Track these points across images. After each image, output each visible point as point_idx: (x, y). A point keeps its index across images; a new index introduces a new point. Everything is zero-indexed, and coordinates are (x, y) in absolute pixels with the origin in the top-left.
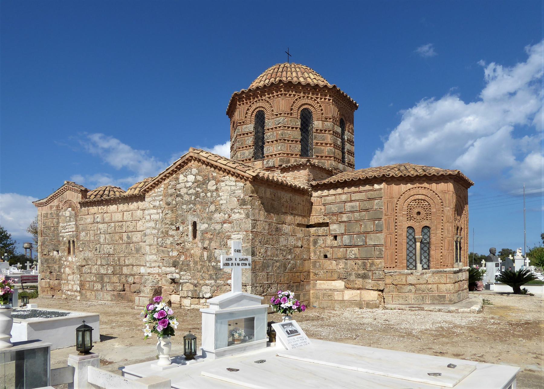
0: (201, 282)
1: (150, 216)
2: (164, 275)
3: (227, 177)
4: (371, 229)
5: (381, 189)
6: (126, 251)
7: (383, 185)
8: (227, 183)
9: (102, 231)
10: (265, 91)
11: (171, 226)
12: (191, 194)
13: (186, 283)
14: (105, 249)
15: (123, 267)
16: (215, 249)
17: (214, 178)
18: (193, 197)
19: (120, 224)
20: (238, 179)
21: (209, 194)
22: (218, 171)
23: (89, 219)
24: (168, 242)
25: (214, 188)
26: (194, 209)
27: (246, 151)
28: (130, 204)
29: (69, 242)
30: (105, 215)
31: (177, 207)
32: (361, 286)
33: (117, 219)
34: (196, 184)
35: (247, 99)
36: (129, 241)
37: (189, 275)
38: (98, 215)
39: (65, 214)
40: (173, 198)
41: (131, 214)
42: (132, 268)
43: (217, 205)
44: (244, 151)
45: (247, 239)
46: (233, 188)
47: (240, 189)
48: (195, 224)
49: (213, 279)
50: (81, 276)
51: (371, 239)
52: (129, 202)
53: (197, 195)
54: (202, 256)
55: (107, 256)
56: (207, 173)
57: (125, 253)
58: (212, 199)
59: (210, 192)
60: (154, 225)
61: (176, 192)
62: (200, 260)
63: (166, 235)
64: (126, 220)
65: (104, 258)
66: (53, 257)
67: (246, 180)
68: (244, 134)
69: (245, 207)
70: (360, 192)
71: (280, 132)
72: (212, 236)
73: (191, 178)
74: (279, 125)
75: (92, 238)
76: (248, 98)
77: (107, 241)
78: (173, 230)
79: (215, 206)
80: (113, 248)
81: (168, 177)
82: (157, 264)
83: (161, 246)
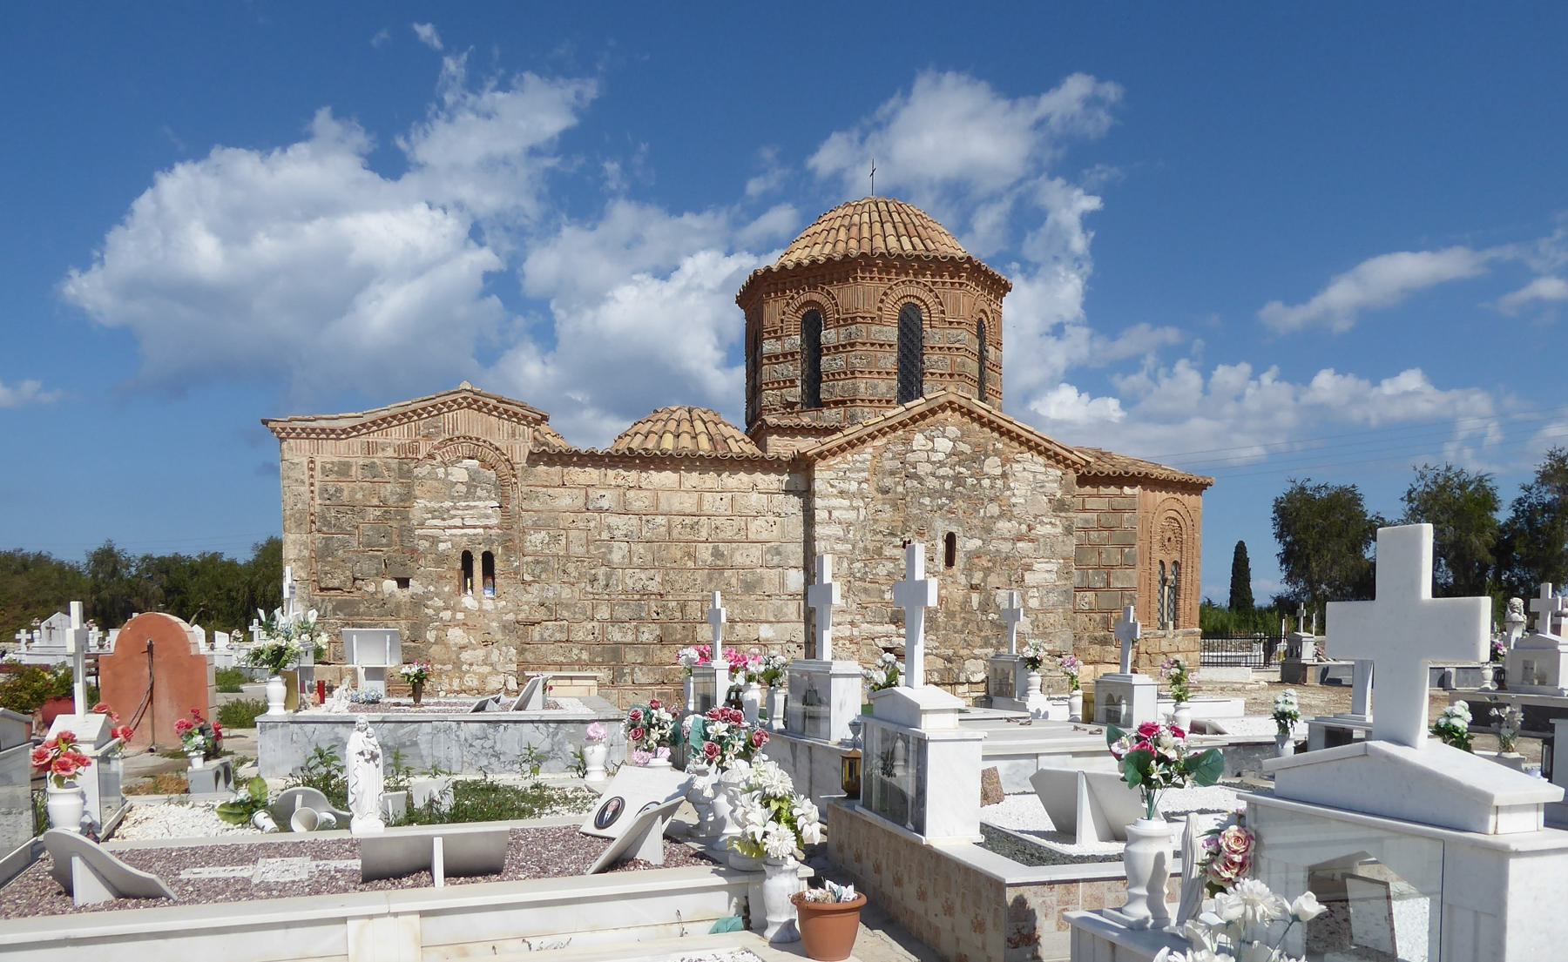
0: (964, 652)
2: (866, 641)
3: (1028, 455)
4: (1117, 561)
5: (1134, 496)
7: (1137, 490)
8: (1028, 465)
10: (929, 268)
11: (889, 538)
12: (943, 477)
15: (698, 625)
17: (997, 453)
18: (948, 485)
19: (688, 520)
20: (1050, 462)
21: (986, 483)
23: (565, 499)
25: (999, 471)
26: (951, 508)
27: (880, 381)
29: (467, 558)
30: (631, 494)
31: (908, 499)
32: (1097, 658)
34: (956, 459)
35: (883, 271)
40: (898, 479)
43: (1004, 506)
44: (876, 381)
45: (1065, 572)
46: (1040, 477)
47: (1056, 481)
48: (950, 540)
49: (992, 646)
50: (521, 652)
51: (1117, 578)
53: (958, 480)
55: (636, 597)
56: (982, 441)
57: (705, 593)
58: (993, 491)
59: (988, 478)
60: (841, 533)
61: (904, 468)
62: (961, 608)
64: (708, 513)
66: (380, 596)
67: (1067, 466)
68: (872, 345)
69: (1063, 514)
70: (1099, 496)
71: (959, 360)
72: (990, 564)
73: (944, 445)
74: (957, 345)
76: (887, 268)
77: (635, 559)
78: (895, 546)
79: (1000, 506)
81: (884, 434)
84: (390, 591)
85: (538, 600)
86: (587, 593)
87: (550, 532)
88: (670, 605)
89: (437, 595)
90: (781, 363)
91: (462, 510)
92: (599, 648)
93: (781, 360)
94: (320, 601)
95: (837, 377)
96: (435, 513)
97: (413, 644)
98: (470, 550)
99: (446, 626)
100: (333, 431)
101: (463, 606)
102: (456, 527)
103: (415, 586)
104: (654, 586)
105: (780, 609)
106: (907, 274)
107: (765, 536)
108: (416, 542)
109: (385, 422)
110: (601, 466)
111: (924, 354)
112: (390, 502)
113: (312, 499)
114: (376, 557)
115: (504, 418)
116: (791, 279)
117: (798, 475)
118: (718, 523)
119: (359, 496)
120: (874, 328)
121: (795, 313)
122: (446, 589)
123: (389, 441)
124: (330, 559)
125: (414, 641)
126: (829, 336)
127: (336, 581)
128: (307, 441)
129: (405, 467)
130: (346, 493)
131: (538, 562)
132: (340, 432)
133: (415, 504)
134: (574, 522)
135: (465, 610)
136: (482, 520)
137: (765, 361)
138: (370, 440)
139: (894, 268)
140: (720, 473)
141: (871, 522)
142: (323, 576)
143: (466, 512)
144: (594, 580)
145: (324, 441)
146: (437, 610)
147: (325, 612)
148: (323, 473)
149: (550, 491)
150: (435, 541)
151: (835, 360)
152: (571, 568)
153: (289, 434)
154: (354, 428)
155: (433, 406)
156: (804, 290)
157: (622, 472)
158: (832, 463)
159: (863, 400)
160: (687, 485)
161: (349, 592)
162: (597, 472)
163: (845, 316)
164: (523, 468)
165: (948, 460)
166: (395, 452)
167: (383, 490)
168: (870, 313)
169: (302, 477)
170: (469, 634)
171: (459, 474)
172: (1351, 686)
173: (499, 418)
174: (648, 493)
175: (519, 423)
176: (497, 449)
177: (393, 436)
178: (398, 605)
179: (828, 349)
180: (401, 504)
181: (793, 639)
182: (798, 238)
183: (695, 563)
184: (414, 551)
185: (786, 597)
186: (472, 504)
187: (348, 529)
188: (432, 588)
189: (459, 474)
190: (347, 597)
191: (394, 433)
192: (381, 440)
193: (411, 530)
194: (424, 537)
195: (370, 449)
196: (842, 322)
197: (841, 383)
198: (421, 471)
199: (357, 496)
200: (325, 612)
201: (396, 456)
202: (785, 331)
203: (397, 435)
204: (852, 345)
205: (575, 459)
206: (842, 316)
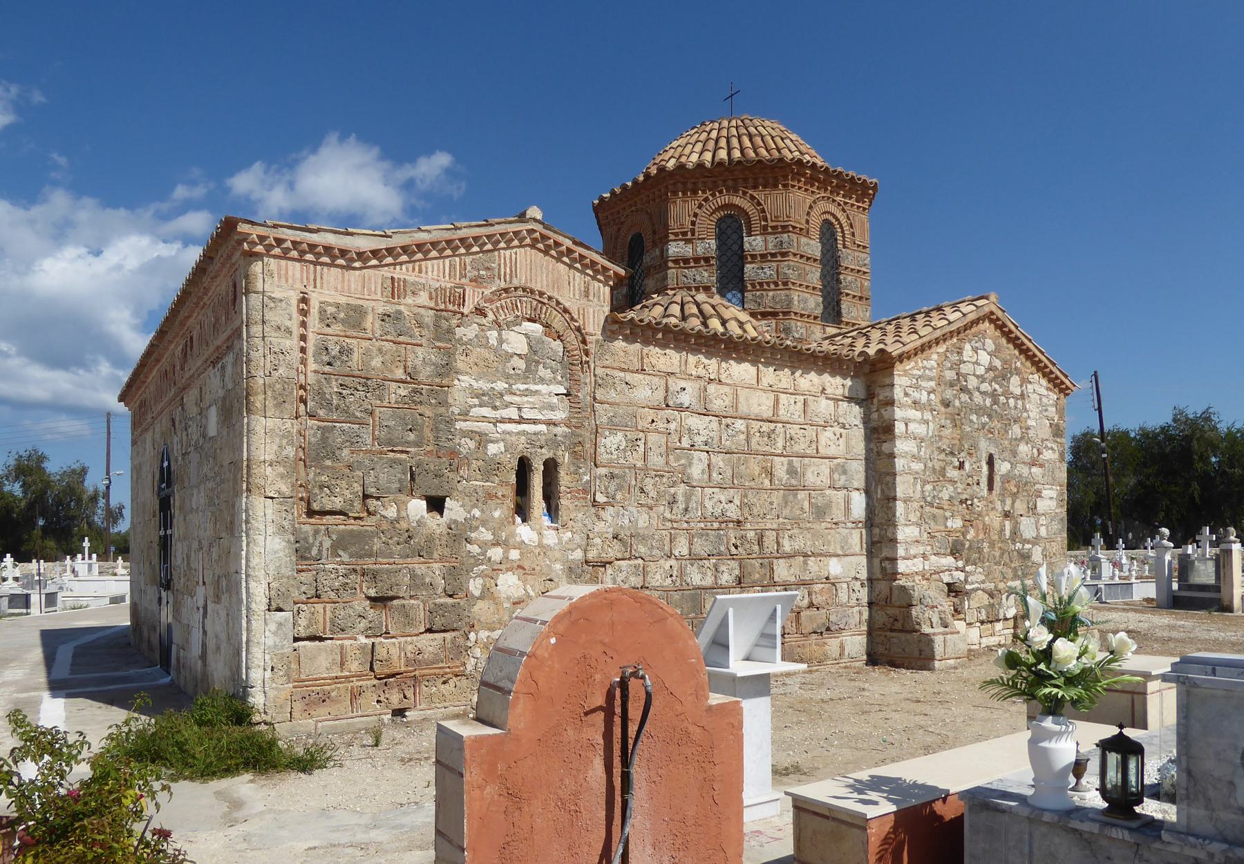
0: (1001, 586)
1: (906, 424)
3: (1036, 376)
6: (786, 512)
9: (699, 440)
13: (978, 589)
14: (708, 504)
15: (775, 561)
16: (1021, 515)
19: (766, 427)
22: (1024, 360)
23: (645, 391)
24: (945, 495)
28: (798, 373)
30: (712, 388)
33: (755, 410)
36: (794, 482)
37: (980, 573)
38: (683, 384)
39: (501, 341)
40: (955, 392)
41: (800, 405)
42: (805, 563)
52: (799, 368)
54: (1002, 530)
55: (716, 525)
57: (781, 520)
60: (915, 450)
63: (942, 479)
64: (785, 419)
65: (703, 534)
66: (404, 525)
68: (802, 256)
69: (1059, 440)
75: (656, 461)
77: (714, 475)
80: (737, 502)
82: (921, 549)
83: (931, 505)
84: (418, 518)
85: (611, 530)
86: (665, 519)
87: (628, 434)
88: (748, 535)
89: (484, 523)
90: (692, 267)
91: (520, 395)
92: (676, 596)
93: (692, 264)
94: (311, 533)
95: (765, 287)
96: (484, 398)
97: (450, 601)
98: (529, 455)
99: (496, 569)
100: (343, 253)
101: (518, 539)
102: (511, 421)
103: (454, 509)
104: (733, 512)
105: (845, 540)
106: (826, 190)
107: (832, 451)
108: (457, 441)
109: (420, 251)
110: (684, 349)
111: (840, 273)
112: (421, 377)
113: (303, 362)
114: (400, 462)
115: (576, 269)
116: (706, 179)
117: (858, 380)
118: (793, 433)
119: (376, 362)
120: (803, 240)
121: (711, 215)
122: (497, 514)
123: (423, 281)
124: (328, 463)
125: (451, 596)
126: (754, 243)
127: (337, 500)
128: (298, 264)
129: (444, 324)
130: (355, 356)
131: (612, 476)
132: (355, 256)
133: (456, 382)
134: (653, 421)
135: (521, 545)
136: (545, 412)
137: (670, 264)
138: (396, 276)
139: (817, 181)
140: (793, 370)
141: (937, 438)
142: (316, 491)
143: (525, 399)
144: (672, 502)
145: (325, 269)
146: (484, 546)
147: (320, 551)
148: (321, 320)
149: (629, 377)
150: (482, 440)
151: (763, 269)
152: (649, 484)
153: (269, 248)
154: (375, 253)
155: (489, 237)
156: (721, 192)
157: (703, 360)
158: (908, 368)
159: (796, 314)
160: (765, 382)
161: (355, 518)
162: (678, 355)
163: (774, 224)
164: (597, 341)
165: (988, 375)
166: (431, 298)
167: (411, 357)
168: (800, 223)
169: (288, 323)
170: (525, 582)
171: (516, 342)
173: (570, 267)
174: (726, 389)
175: (594, 278)
176: (566, 311)
177: (430, 273)
178: (430, 539)
179: (754, 257)
180: (438, 380)
181: (858, 576)
182: (667, 149)
183: (771, 481)
184: (453, 453)
185: (850, 525)
186: (533, 387)
187: (358, 414)
188: (477, 513)
189: (516, 342)
190: (354, 526)
191: (430, 270)
192: (411, 278)
193: (450, 422)
194: (470, 434)
195: (396, 289)
196: (770, 230)
197: (771, 294)
198: (468, 332)
199: (373, 363)
200: (320, 551)
201: (432, 305)
202: (697, 234)
203: (435, 273)
204: (784, 254)
205: (660, 336)
206: (771, 224)
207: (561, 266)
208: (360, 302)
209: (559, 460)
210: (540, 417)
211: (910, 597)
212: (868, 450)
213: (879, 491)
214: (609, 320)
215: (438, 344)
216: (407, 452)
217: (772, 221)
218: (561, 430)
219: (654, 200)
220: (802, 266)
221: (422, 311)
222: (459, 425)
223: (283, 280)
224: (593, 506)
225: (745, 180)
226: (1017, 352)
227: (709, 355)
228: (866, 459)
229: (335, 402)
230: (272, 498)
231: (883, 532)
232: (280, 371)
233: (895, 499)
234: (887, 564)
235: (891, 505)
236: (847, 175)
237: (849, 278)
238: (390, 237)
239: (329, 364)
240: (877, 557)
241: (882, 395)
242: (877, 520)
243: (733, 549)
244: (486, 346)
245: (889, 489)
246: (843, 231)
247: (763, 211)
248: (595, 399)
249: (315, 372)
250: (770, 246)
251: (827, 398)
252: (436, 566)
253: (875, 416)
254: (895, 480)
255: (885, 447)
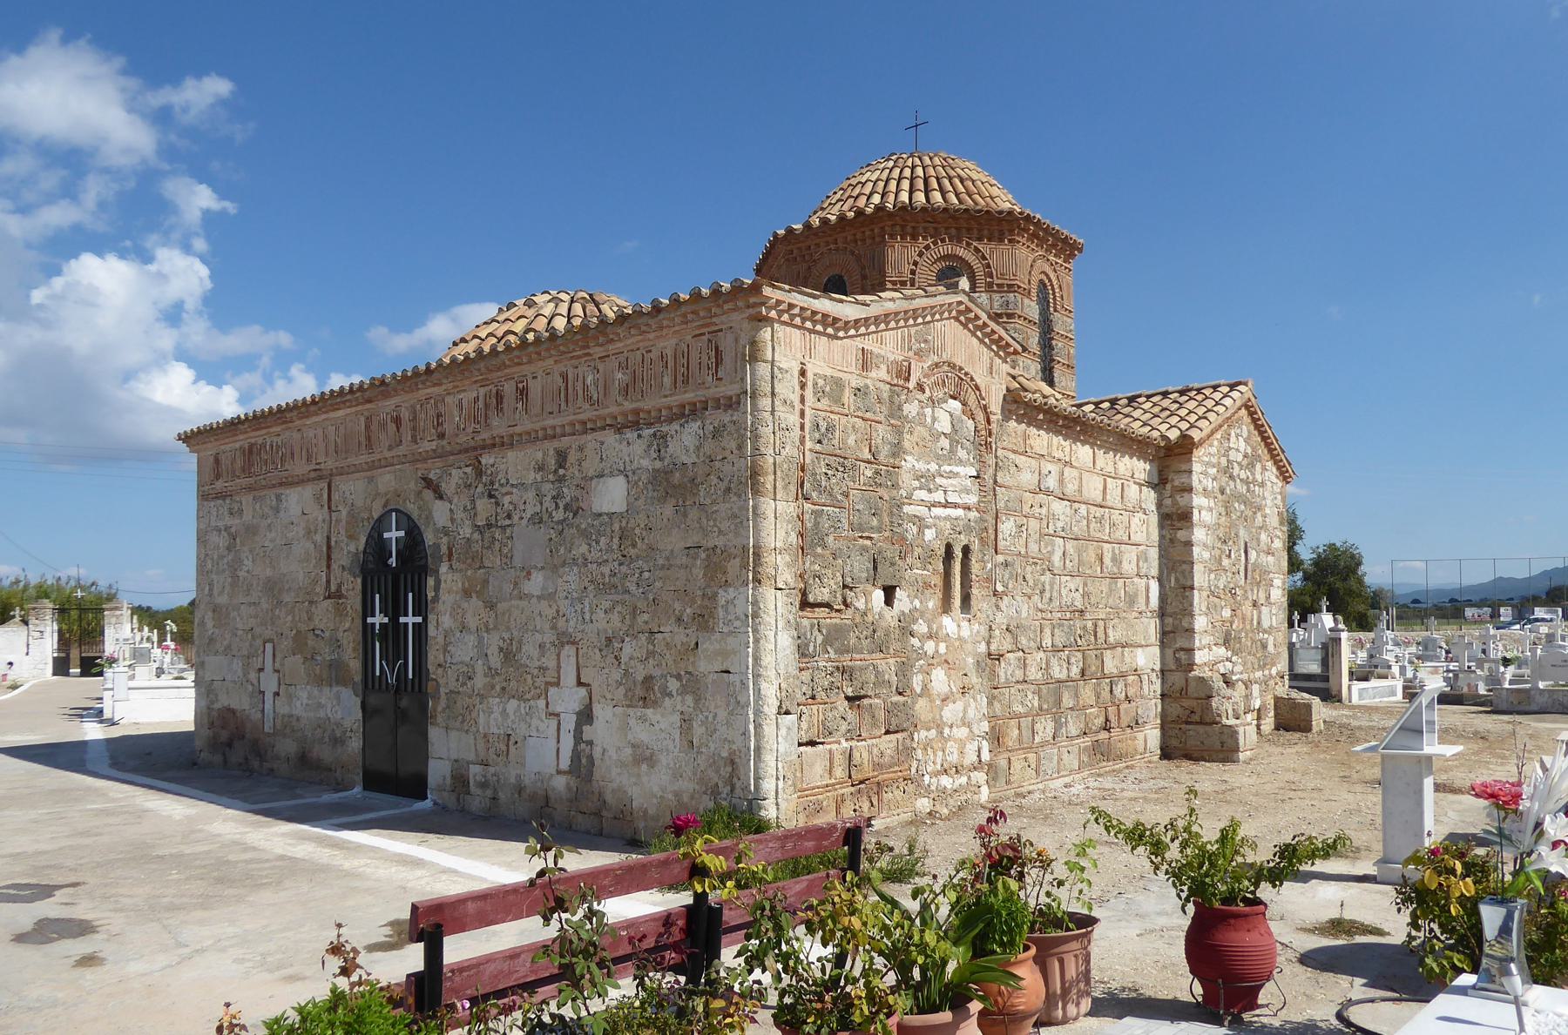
30: (1067, 470)
66: (870, 618)
68: (1025, 319)
106: (1042, 248)
111: (1053, 339)
115: (985, 344)
119: (851, 441)
123: (883, 353)
125: (900, 694)
133: (903, 463)
143: (950, 481)
156: (943, 241)
163: (1000, 282)
172: (129, 689)
173: (982, 341)
188: (917, 603)
196: (995, 288)
201: (889, 380)
204: (1010, 316)
207: (975, 341)
208: (841, 375)
209: (972, 547)
210: (959, 501)
211: (1211, 688)
212: (1162, 537)
213: (1173, 580)
214: (1008, 398)
215: (892, 422)
216: (870, 538)
217: (998, 278)
218: (973, 515)
219: (863, 240)
220: (1025, 329)
221: (882, 385)
222: (906, 509)
223: (788, 349)
224: (995, 595)
225: (969, 230)
226: (1259, 439)
227: (1066, 438)
228: (1159, 546)
229: (823, 483)
230: (780, 589)
231: (1178, 622)
232: (787, 449)
233: (1192, 588)
234: (1182, 655)
235: (1187, 594)
236: (1053, 229)
237: (1060, 344)
238: (868, 305)
239: (820, 442)
240: (1170, 647)
241: (1178, 481)
242: (1169, 610)
243: (1078, 640)
244: (923, 424)
245: (1184, 577)
246: (1054, 294)
247: (988, 266)
248: (995, 482)
249: (811, 450)
250: (996, 305)
251: (1135, 483)
252: (892, 661)
253: (1168, 502)
254: (1192, 568)
255: (1181, 535)
